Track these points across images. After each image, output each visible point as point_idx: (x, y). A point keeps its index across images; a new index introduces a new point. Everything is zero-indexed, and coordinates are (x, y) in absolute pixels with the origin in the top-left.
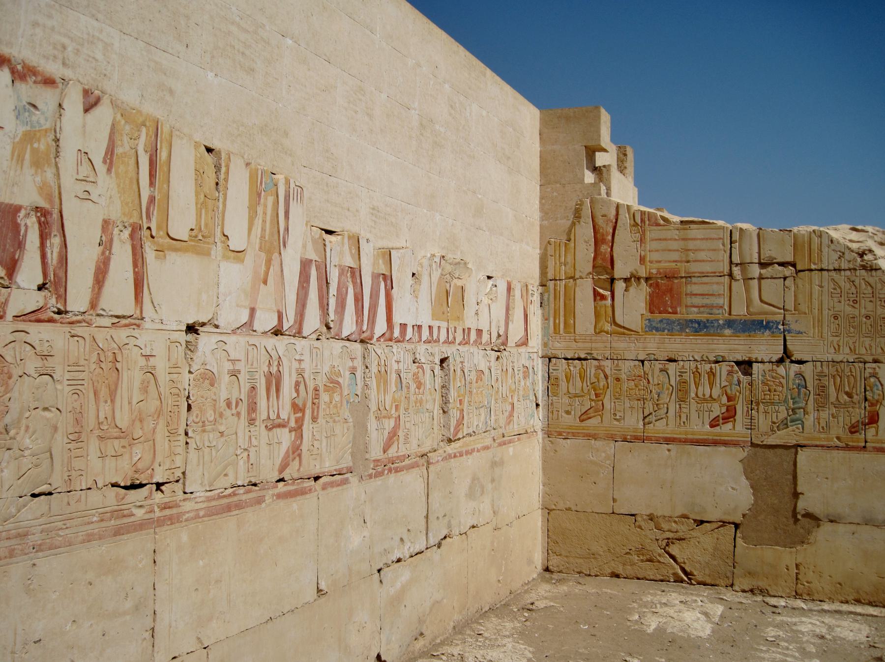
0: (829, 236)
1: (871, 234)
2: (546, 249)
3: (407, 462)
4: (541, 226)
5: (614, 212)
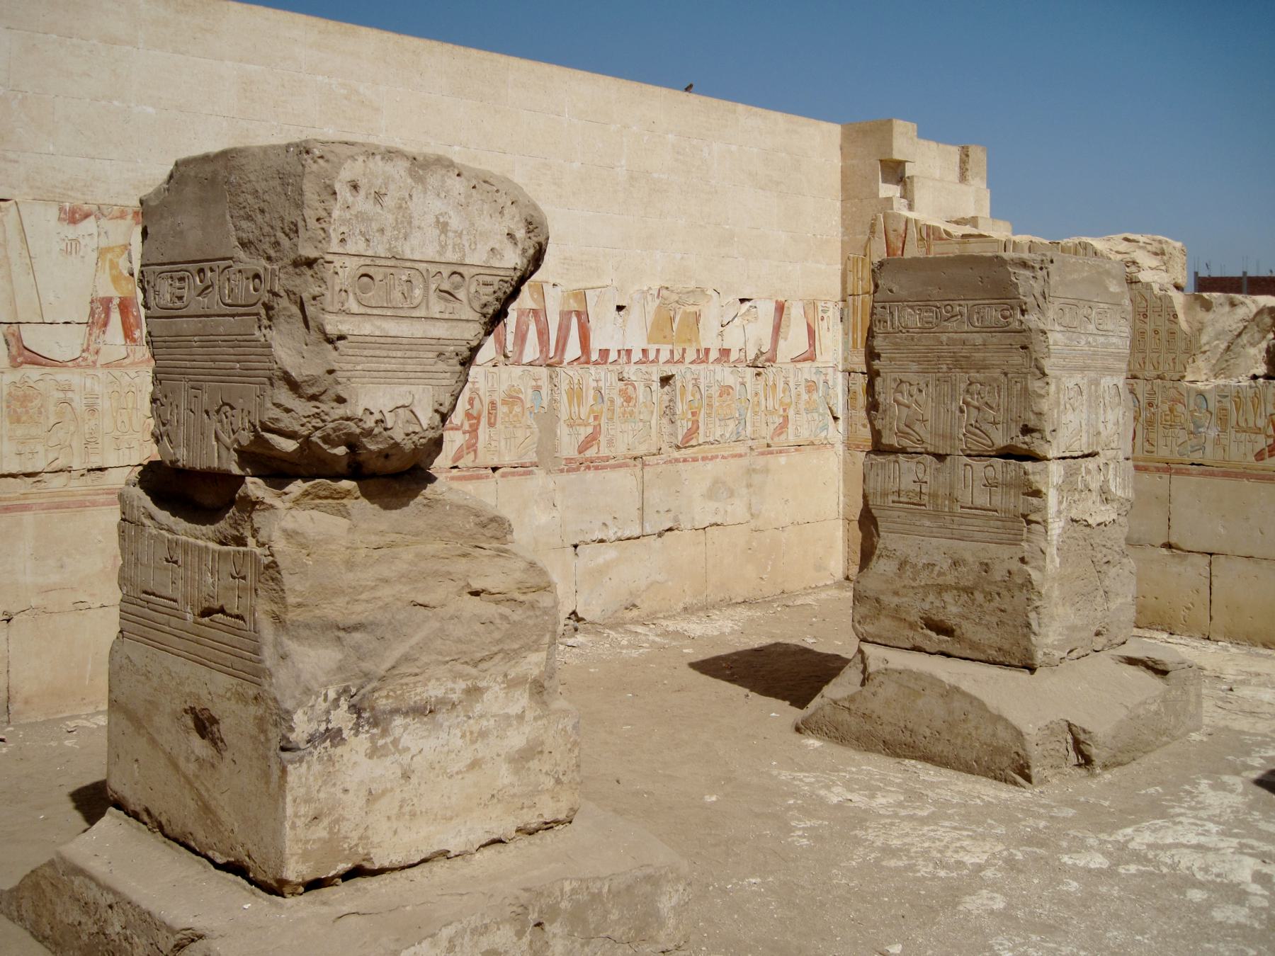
0: (1093, 248)
1: (1141, 244)
2: (846, 265)
3: (612, 462)
4: (842, 242)
5: (903, 227)
